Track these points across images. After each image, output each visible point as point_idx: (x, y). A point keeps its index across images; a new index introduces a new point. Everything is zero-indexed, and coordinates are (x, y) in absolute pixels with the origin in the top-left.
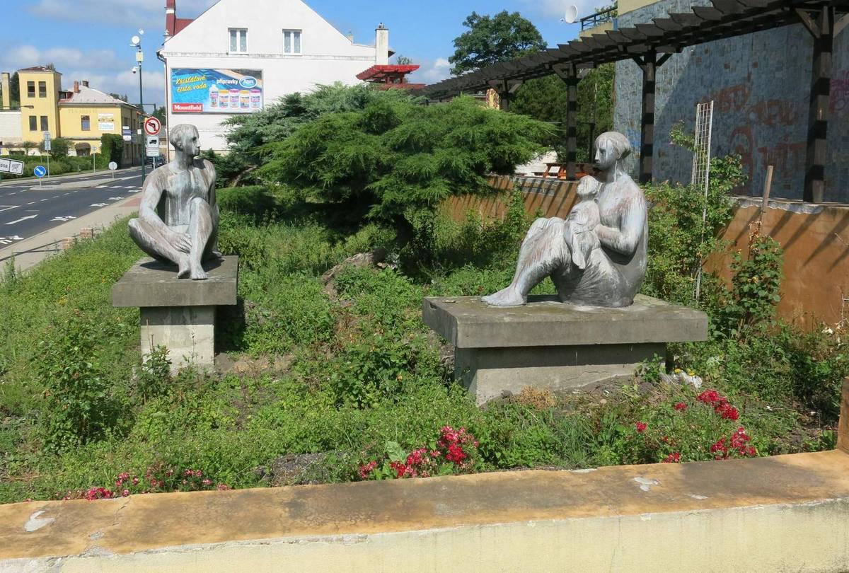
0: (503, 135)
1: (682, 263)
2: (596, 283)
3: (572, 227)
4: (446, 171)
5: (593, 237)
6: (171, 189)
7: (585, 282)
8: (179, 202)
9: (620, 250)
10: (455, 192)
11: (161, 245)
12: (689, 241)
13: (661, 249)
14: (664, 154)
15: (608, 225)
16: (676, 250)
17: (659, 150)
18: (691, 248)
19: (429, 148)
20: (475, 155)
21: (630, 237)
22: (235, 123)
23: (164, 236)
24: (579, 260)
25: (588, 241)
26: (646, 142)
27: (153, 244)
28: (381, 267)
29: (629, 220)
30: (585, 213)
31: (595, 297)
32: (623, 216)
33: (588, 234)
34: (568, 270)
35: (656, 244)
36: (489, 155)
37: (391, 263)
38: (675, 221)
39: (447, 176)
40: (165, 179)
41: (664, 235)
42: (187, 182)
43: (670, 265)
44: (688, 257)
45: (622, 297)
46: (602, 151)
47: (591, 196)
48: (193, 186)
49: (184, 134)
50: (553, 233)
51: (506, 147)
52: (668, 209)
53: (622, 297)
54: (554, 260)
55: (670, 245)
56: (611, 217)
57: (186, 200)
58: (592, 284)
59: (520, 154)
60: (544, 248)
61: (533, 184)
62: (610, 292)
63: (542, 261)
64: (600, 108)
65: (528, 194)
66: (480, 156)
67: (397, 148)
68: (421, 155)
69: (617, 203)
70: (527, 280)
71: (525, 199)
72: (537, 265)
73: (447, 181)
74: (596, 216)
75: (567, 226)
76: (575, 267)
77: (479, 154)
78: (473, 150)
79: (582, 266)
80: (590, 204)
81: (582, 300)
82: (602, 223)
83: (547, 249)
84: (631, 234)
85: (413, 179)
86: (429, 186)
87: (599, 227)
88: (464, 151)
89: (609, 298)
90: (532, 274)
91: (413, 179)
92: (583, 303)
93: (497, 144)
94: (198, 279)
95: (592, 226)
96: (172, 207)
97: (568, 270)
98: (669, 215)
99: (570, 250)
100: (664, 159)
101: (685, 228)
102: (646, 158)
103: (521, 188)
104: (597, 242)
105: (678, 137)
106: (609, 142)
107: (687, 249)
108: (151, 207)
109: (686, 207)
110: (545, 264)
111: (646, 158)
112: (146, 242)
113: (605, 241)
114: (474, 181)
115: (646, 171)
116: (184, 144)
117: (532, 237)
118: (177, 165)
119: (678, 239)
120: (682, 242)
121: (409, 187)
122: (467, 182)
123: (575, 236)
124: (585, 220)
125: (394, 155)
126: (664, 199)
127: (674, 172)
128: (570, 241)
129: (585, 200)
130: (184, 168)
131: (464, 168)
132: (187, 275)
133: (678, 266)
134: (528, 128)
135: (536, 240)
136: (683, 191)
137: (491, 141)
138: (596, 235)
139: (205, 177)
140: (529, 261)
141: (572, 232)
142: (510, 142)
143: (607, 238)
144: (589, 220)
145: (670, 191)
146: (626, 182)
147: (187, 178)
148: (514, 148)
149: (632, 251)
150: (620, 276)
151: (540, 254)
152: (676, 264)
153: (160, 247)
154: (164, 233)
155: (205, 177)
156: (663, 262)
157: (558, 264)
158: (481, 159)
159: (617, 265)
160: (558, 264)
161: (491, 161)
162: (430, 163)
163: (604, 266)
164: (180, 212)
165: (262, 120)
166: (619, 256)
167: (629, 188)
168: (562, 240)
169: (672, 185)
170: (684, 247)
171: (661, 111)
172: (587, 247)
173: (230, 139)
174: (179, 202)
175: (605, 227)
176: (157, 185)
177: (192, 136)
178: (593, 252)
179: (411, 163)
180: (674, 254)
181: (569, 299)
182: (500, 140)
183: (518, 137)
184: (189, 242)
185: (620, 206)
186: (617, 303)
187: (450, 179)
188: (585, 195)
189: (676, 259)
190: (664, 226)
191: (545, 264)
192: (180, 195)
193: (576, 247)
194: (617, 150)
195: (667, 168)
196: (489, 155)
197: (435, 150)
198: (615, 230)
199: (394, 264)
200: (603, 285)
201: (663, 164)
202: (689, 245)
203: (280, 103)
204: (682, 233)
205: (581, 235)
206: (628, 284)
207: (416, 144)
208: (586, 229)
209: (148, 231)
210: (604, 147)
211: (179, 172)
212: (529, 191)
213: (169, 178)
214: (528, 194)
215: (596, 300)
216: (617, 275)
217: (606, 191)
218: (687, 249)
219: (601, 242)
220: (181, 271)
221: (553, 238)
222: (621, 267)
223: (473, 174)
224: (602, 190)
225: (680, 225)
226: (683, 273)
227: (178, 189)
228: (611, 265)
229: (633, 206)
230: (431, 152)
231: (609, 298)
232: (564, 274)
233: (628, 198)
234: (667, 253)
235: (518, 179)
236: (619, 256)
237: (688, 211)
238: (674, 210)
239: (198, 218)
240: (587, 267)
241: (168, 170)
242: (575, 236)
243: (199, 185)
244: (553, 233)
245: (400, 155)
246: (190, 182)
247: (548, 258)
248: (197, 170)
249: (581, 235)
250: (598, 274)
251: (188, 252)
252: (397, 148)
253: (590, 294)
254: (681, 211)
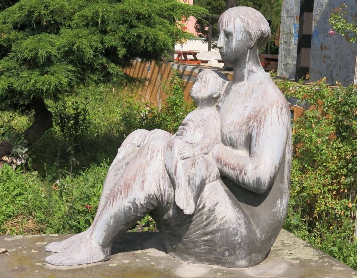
0: (139, 17)
1: (339, 183)
2: (212, 233)
3: (176, 149)
4: (70, 55)
5: (207, 165)
7: (194, 232)
9: (248, 185)
10: (82, 80)
12: (349, 157)
13: (314, 163)
14: (326, 48)
15: (233, 145)
16: (333, 167)
17: (322, 43)
18: (350, 166)
19: (55, 28)
20: (106, 38)
21: (262, 167)
24: (185, 203)
25: (199, 172)
26: (305, 32)
28: (6, 161)
29: (261, 139)
30: (201, 125)
31: (209, 252)
32: (254, 134)
33: (200, 160)
34: (171, 212)
35: (304, 155)
36: (123, 38)
37: (17, 157)
38: (332, 129)
39: (71, 62)
41: (317, 148)
43: (324, 186)
44: (346, 176)
45: (249, 254)
46: (228, 35)
47: (212, 100)
50: (149, 156)
51: (142, 29)
52: (324, 114)
53: (249, 254)
54: (149, 198)
55: (325, 161)
56: (237, 135)
58: (206, 234)
59: (157, 39)
60: (134, 179)
61: (192, 72)
62: (232, 248)
63: (130, 198)
64: (276, 8)
65: (187, 82)
66: (111, 40)
67: (21, 27)
68: (43, 35)
69: (246, 115)
70: (108, 225)
71: (185, 87)
72: (122, 204)
73: (71, 67)
74: (215, 133)
75: (170, 146)
76: (179, 211)
77: (111, 37)
78: (104, 32)
79: (188, 210)
80: (208, 111)
81: (191, 255)
82: (224, 141)
83: (139, 181)
84: (260, 166)
85: (32, 63)
86: (47, 73)
87: (220, 149)
88: (92, 33)
89: (230, 255)
90: (116, 217)
91: (32, 63)
92: (193, 259)
93: (132, 27)
95: (207, 147)
97: (171, 212)
98: (324, 121)
99: (173, 184)
100: (325, 52)
101: (344, 139)
102: (303, 50)
103: (181, 76)
104: (215, 172)
105: (340, 25)
106: (238, 21)
107: (346, 167)
109: (347, 113)
110: (134, 203)
111: (303, 50)
113: (226, 170)
114: (104, 68)
115: (303, 64)
117: (123, 159)
119: (334, 152)
120: (339, 157)
121: (26, 73)
122: (96, 69)
123: (181, 163)
124: (198, 137)
125: (14, 34)
126: (320, 101)
127: (335, 66)
128: (172, 171)
129: (202, 106)
131: (89, 53)
133: (335, 187)
134: (172, 10)
135: (127, 164)
136: (343, 92)
137: (125, 22)
138: (213, 162)
140: (113, 197)
141: (177, 156)
142: (148, 25)
143: (230, 167)
144: (204, 137)
145: (327, 91)
146: (260, 83)
148: (151, 32)
149: (265, 187)
150: (248, 224)
151: (128, 187)
152: (332, 184)
156: (314, 182)
157: (155, 203)
158: (114, 44)
159: (243, 205)
160: (155, 203)
161: (124, 46)
162: (49, 44)
163: (224, 210)
166: (245, 194)
167: (265, 92)
168: (162, 167)
169: (331, 81)
170: (342, 163)
171: (324, 7)
172: (198, 182)
175: (229, 148)
178: (207, 188)
179: (27, 44)
180: (329, 172)
181: (174, 250)
182: (134, 22)
183: (158, 19)
185: (250, 118)
186: (243, 262)
187: (75, 65)
188: (203, 100)
189: (332, 179)
190: (319, 136)
191: (134, 203)
193: (181, 179)
194: (249, 34)
195: (328, 61)
196: (123, 38)
197: (62, 30)
198: (242, 153)
199: (21, 159)
200: (222, 237)
201: (324, 57)
202: (348, 162)
204: (341, 145)
205: (189, 161)
206: (259, 236)
207: (39, 23)
208: (197, 151)
210: (230, 28)
212: (189, 80)
214: (187, 82)
215: (211, 257)
216: (242, 222)
217: (232, 93)
218: (346, 167)
219: (221, 171)
221: (148, 163)
222: (249, 209)
223: (105, 60)
224: (227, 92)
225: (338, 133)
226: (339, 195)
228: (235, 205)
229: (268, 118)
230: (57, 33)
231: (230, 255)
232: (165, 217)
233: (262, 107)
234: (321, 171)
235: (179, 67)
236: (245, 194)
237: (348, 118)
238: (332, 115)
240: (198, 210)
242: (181, 163)
244: (149, 156)
245: (20, 34)
247: (139, 197)
249: (189, 161)
250: (214, 221)
252: (21, 27)
253: (203, 248)
254: (340, 118)
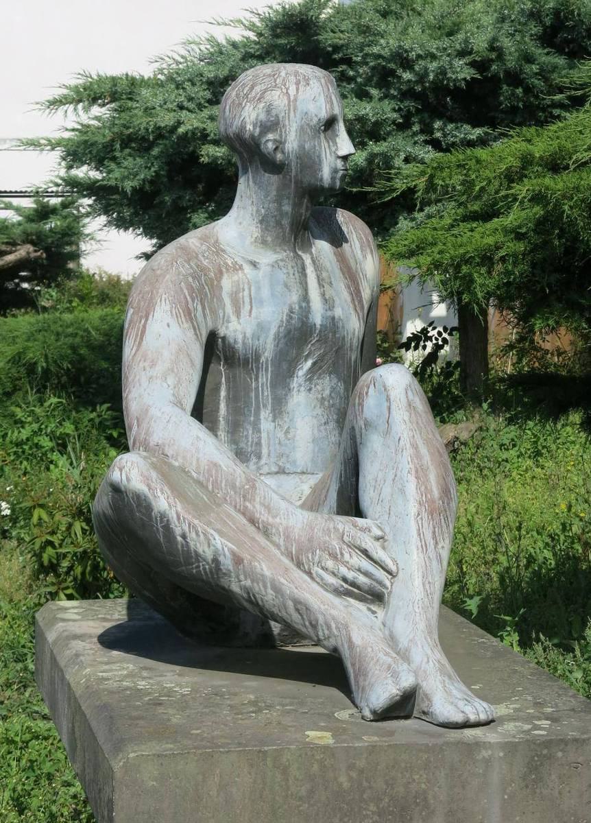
6: (237, 329)
8: (265, 379)
11: (265, 568)
22: (94, 100)
23: (266, 532)
27: (227, 562)
40: (215, 287)
42: (294, 297)
48: (318, 316)
49: (292, 103)
57: (291, 373)
94: (466, 725)
96: (233, 399)
108: (179, 404)
112: (191, 557)
116: (292, 144)
118: (255, 231)
130: (281, 241)
132: (404, 706)
139: (351, 276)
147: (293, 281)
153: (257, 578)
154: (263, 516)
155: (351, 276)
164: (266, 424)
165: (192, 90)
173: (76, 153)
174: (265, 379)
176: (189, 315)
177: (324, 114)
184: (379, 554)
192: (268, 354)
203: (238, 34)
209: (199, 509)
211: (267, 258)
213: (227, 283)
220: (381, 693)
227: (261, 327)
239: (409, 452)
241: (218, 250)
243: (338, 312)
246: (305, 298)
248: (322, 247)
251: (375, 597)
